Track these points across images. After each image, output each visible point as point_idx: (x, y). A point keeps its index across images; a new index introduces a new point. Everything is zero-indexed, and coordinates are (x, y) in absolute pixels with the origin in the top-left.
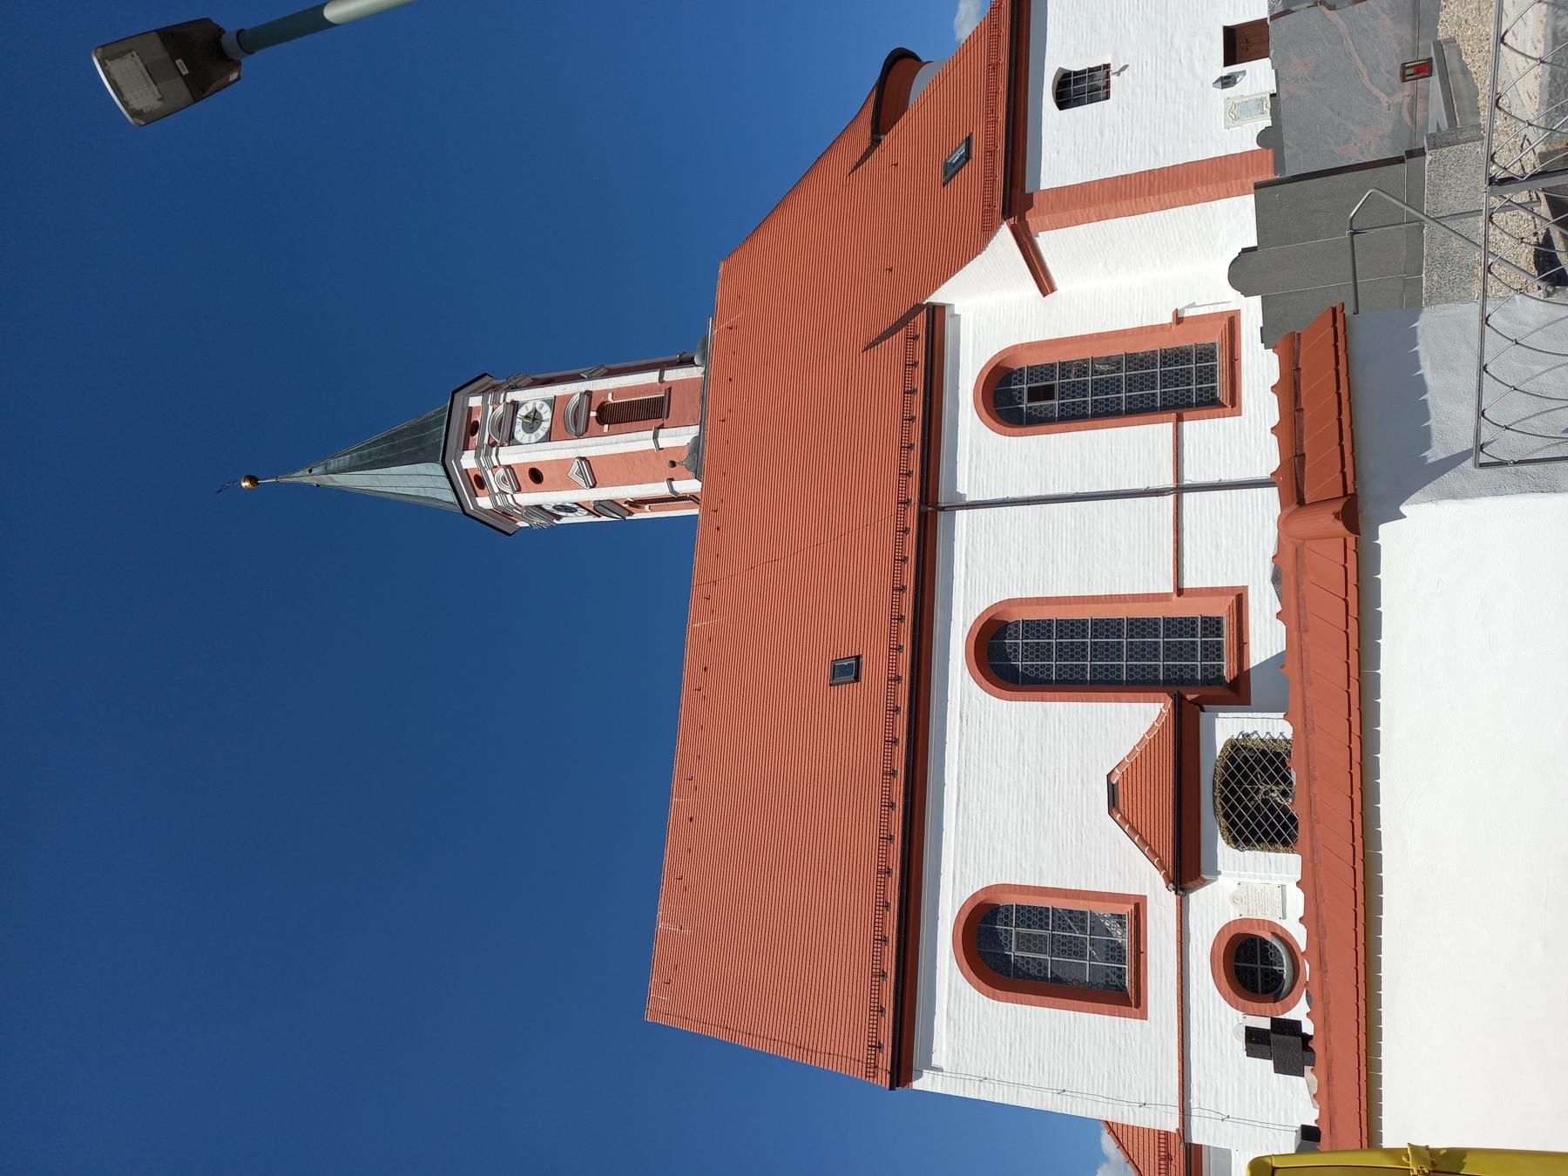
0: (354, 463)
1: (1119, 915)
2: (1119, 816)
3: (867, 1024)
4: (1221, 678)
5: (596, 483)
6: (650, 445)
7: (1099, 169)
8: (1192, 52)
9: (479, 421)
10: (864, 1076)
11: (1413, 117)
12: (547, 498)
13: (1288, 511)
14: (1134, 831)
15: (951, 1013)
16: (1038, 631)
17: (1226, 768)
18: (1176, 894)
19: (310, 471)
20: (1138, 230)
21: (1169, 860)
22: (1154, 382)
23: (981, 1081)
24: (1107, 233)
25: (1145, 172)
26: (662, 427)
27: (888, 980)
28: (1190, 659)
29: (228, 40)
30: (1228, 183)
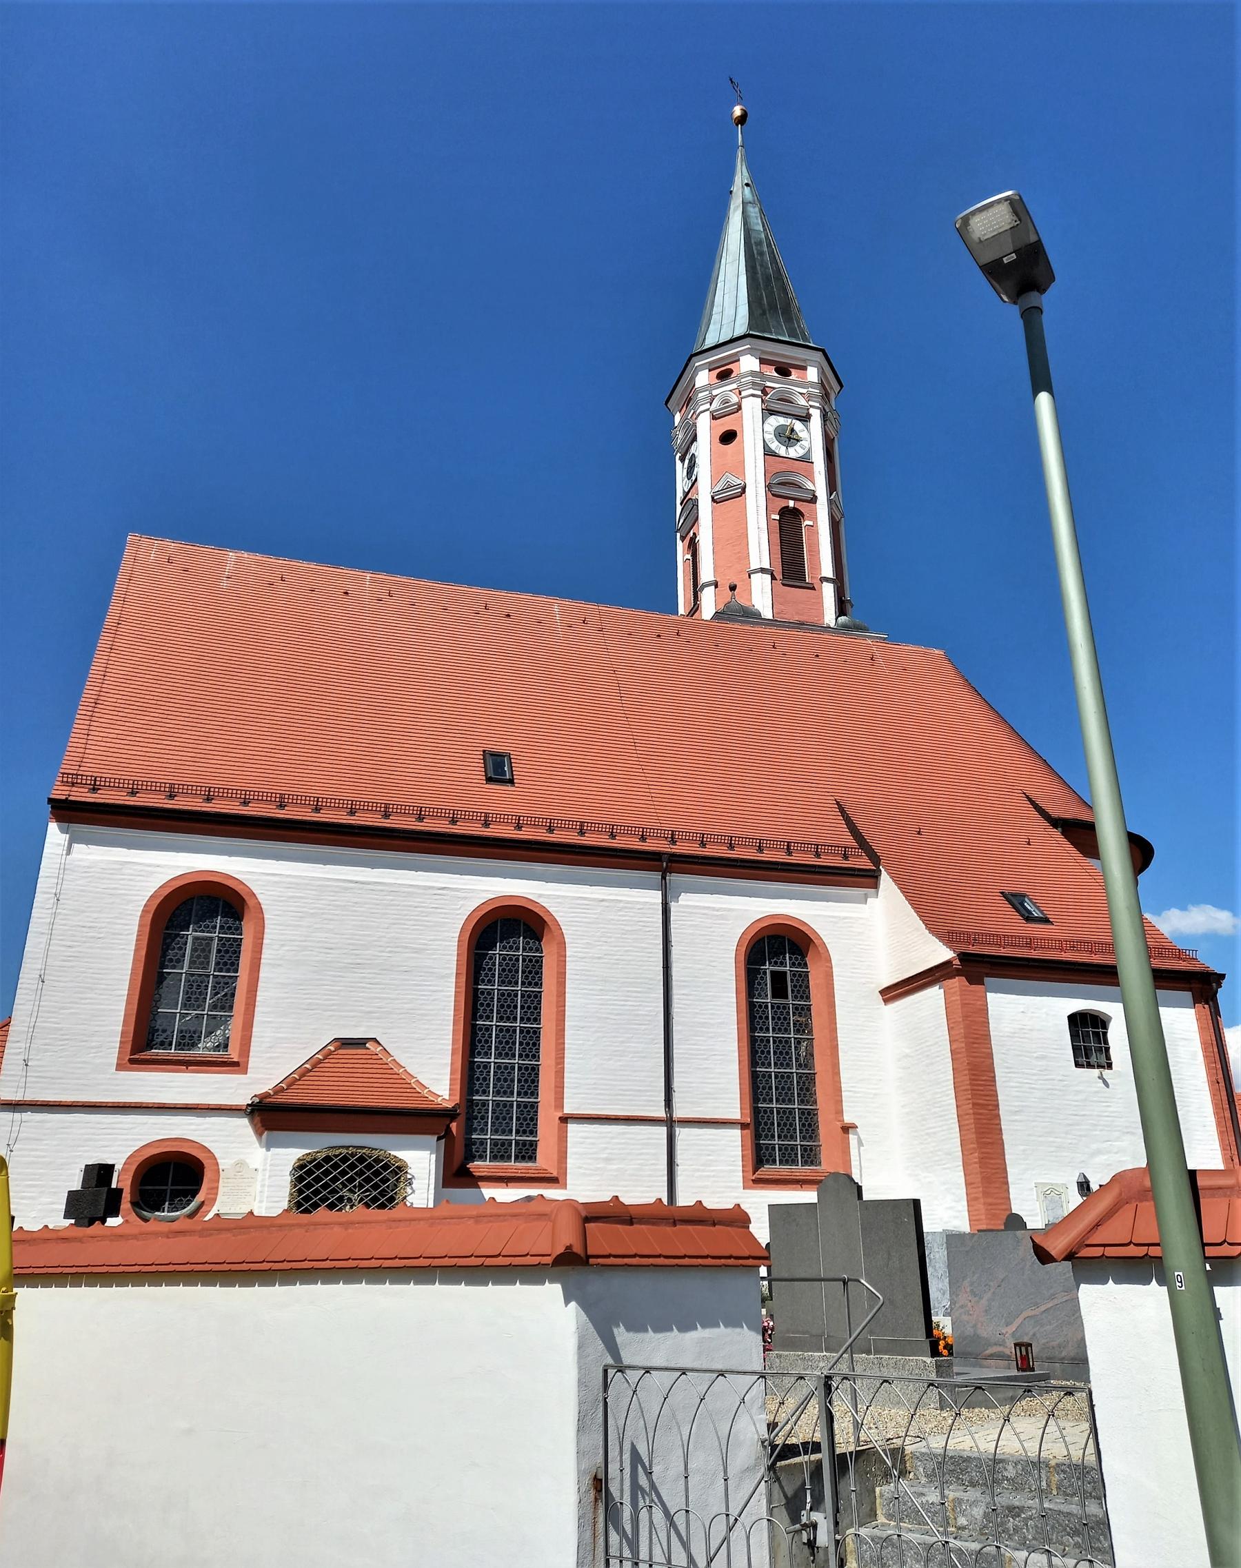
0: (753, 235)
1: (228, 1045)
2: (332, 1048)
3: (119, 777)
4: (472, 1158)
5: (717, 503)
6: (754, 565)
7: (1004, 1053)
8: (1116, 1153)
9: (790, 378)
10: (62, 771)
11: (991, 1356)
12: (703, 448)
13: (580, 1208)
14: (315, 1064)
15: (129, 866)
16: (530, 972)
17: (378, 1160)
18: (248, 1105)
19: (747, 185)
20: (940, 1090)
21: (281, 1099)
22: (784, 1101)
23: (56, 894)
24: (938, 1059)
25: (998, 1100)
26: (773, 578)
27: (166, 801)
28: (493, 1128)
29: (1033, 298)
30: (980, 1185)
